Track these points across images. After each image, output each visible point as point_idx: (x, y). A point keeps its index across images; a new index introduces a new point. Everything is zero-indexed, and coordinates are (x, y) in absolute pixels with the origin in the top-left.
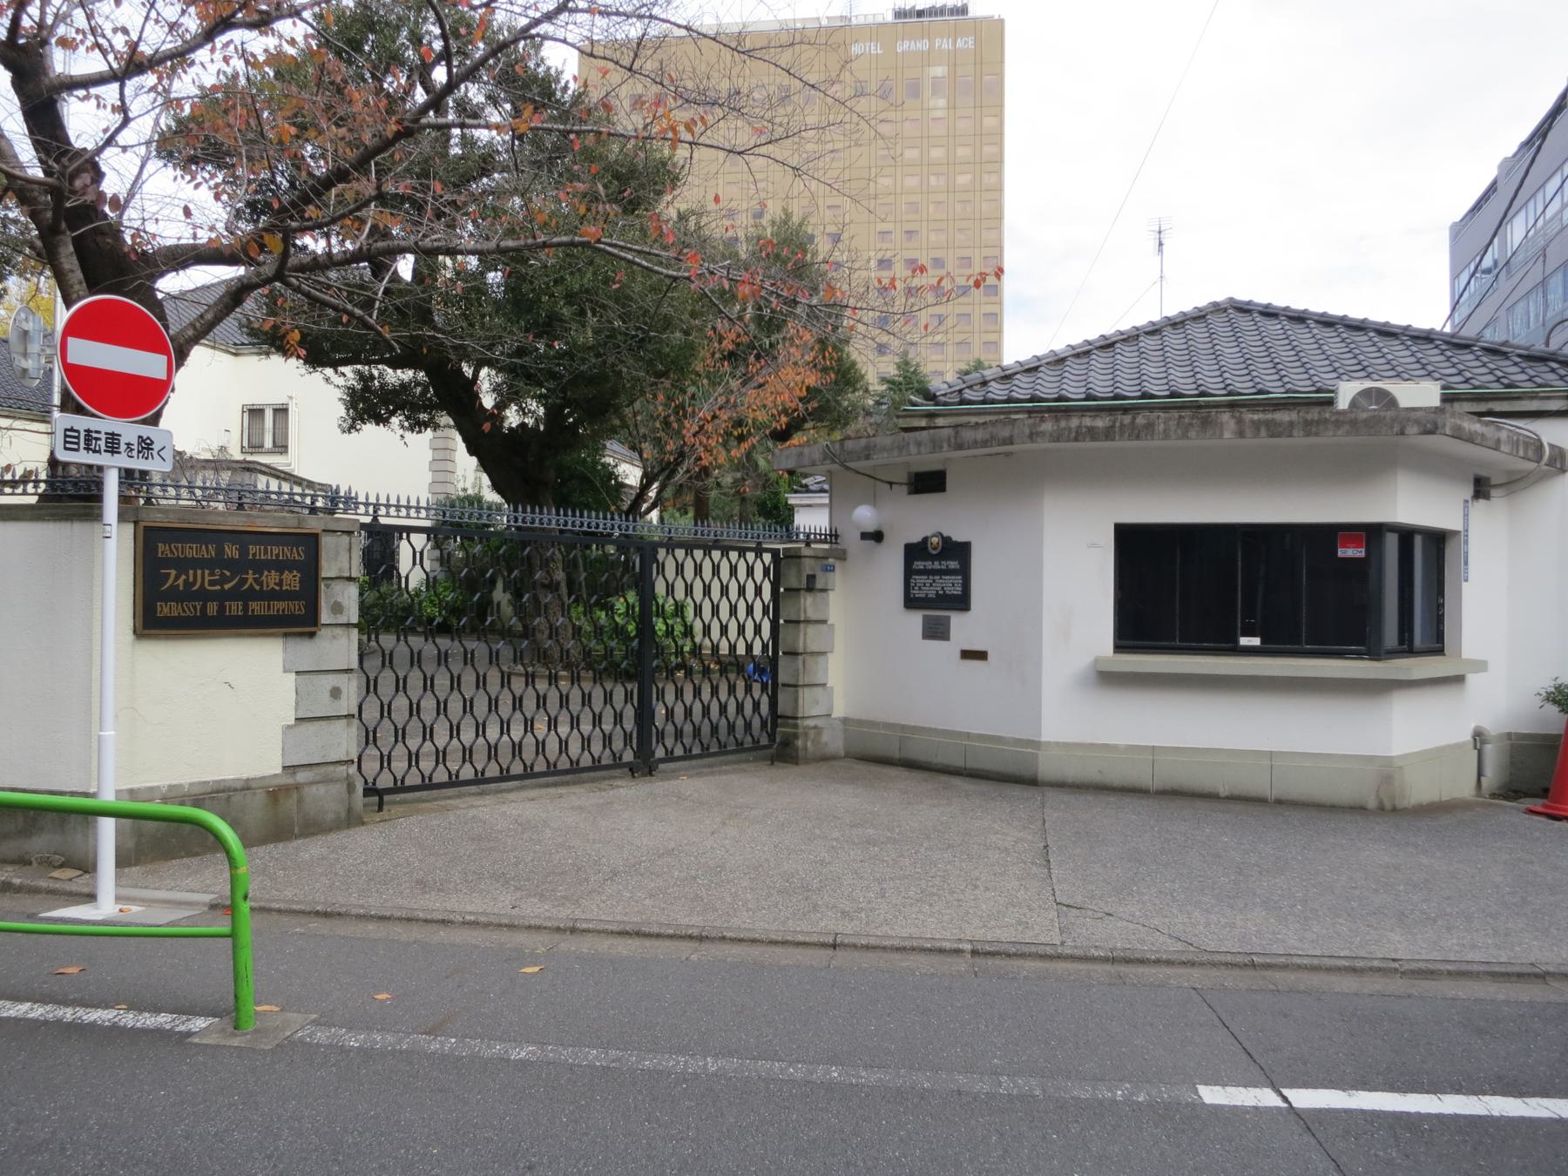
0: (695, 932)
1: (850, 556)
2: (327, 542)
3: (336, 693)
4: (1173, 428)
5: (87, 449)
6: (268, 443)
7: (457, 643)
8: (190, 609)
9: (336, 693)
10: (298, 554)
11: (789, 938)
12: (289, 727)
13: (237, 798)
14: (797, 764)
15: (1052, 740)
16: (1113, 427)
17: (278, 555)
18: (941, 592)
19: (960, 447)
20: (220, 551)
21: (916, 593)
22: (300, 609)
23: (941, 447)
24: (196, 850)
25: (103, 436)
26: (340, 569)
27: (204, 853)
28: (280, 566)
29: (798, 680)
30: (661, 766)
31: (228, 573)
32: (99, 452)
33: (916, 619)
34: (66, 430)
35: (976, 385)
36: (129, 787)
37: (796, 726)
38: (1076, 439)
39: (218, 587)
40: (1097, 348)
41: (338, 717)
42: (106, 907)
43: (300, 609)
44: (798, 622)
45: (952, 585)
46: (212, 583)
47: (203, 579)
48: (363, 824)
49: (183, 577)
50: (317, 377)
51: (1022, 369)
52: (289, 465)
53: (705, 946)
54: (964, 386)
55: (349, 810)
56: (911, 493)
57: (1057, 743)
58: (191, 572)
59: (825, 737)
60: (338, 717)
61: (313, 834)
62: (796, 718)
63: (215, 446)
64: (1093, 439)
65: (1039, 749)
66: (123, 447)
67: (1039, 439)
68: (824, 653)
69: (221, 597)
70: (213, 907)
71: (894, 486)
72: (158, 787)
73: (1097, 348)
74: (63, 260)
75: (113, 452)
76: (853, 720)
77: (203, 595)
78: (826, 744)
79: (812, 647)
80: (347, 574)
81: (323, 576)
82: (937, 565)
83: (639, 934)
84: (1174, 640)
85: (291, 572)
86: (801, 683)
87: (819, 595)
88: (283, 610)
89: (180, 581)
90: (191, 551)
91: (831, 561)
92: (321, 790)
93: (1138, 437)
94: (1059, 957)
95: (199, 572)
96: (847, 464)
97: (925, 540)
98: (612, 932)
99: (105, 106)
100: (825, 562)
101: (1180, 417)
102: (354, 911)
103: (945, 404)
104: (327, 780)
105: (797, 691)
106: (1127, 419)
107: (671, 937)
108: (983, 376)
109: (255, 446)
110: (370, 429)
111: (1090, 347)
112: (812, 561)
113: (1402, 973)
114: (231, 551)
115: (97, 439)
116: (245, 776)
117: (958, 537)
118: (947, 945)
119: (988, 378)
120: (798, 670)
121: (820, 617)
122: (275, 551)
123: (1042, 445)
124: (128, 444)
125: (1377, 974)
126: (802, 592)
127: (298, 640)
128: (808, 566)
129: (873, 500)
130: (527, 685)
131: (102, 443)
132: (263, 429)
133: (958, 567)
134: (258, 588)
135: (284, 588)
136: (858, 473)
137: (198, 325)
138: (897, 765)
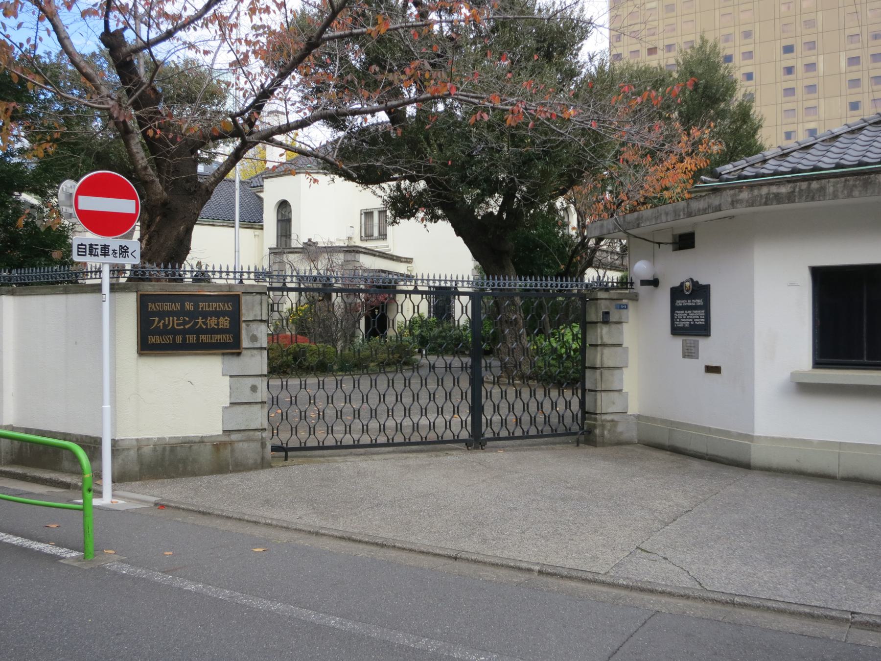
0: (380, 541)
1: (640, 298)
2: (244, 299)
3: (254, 389)
4: (840, 190)
5: (91, 254)
6: (376, 234)
7: (440, 358)
8: (167, 339)
9: (254, 389)
10: (228, 307)
11: (431, 551)
12: (226, 408)
13: (195, 447)
14: (596, 446)
15: (762, 435)
16: (793, 192)
17: (216, 308)
18: (692, 323)
19: (690, 215)
20: (183, 306)
21: (678, 323)
22: (230, 339)
23: (679, 216)
24: (172, 474)
25: (99, 247)
26: (255, 315)
27: (177, 477)
28: (218, 314)
29: (596, 387)
30: (489, 444)
31: (187, 319)
32: (97, 255)
33: (678, 343)
34: (79, 245)
35: (758, 163)
36: (136, 437)
37: (595, 420)
38: (766, 204)
39: (182, 327)
40: (870, 125)
41: (256, 403)
42: (107, 499)
43: (230, 339)
44: (597, 345)
45: (697, 317)
46: (178, 325)
47: (173, 322)
48: (271, 467)
49: (163, 322)
50: (368, 192)
51: (800, 147)
52: (388, 247)
53: (384, 550)
54: (746, 165)
55: (263, 458)
56: (674, 250)
57: (766, 438)
58: (167, 319)
59: (620, 428)
60: (256, 403)
61: (240, 471)
62: (596, 414)
63: (344, 237)
64: (779, 203)
65: (752, 442)
66: (111, 252)
67: (738, 205)
68: (620, 368)
69: (184, 332)
70: (156, 504)
71: (661, 245)
72: (152, 438)
73: (870, 125)
74: (133, 147)
75: (105, 255)
76: (643, 416)
77: (174, 332)
78: (621, 433)
79: (608, 363)
80: (260, 318)
81: (243, 319)
82: (689, 303)
83: (350, 539)
84: (862, 358)
85: (224, 317)
86: (599, 389)
87: (614, 326)
88: (220, 340)
89: (161, 324)
90: (167, 307)
91: (625, 301)
92: (245, 445)
93: (813, 199)
94: (595, 582)
95: (171, 318)
96: (628, 231)
97: (682, 284)
98: (336, 537)
99: (200, 52)
100: (619, 302)
101: (846, 180)
102: (216, 512)
103: (727, 180)
104: (249, 440)
105: (596, 395)
106: (804, 185)
107: (367, 543)
108: (764, 156)
109: (368, 236)
110: (404, 222)
111: (864, 124)
112: (607, 302)
113: (852, 623)
114: (189, 306)
115: (96, 249)
116: (201, 435)
117: (702, 282)
118: (524, 565)
119: (767, 158)
120: (596, 380)
121: (616, 342)
122: (215, 306)
123: (740, 210)
124: (114, 251)
125: (831, 622)
126: (599, 325)
127: (230, 357)
128: (603, 306)
129: (652, 258)
130: (573, 394)
131: (99, 251)
132: (373, 224)
133: (702, 304)
134: (204, 327)
135: (220, 327)
136: (636, 237)
137: (216, 174)
138: (667, 450)
